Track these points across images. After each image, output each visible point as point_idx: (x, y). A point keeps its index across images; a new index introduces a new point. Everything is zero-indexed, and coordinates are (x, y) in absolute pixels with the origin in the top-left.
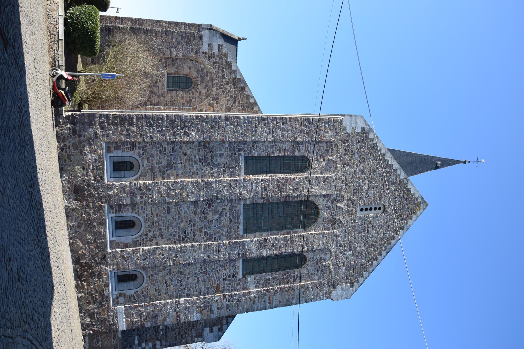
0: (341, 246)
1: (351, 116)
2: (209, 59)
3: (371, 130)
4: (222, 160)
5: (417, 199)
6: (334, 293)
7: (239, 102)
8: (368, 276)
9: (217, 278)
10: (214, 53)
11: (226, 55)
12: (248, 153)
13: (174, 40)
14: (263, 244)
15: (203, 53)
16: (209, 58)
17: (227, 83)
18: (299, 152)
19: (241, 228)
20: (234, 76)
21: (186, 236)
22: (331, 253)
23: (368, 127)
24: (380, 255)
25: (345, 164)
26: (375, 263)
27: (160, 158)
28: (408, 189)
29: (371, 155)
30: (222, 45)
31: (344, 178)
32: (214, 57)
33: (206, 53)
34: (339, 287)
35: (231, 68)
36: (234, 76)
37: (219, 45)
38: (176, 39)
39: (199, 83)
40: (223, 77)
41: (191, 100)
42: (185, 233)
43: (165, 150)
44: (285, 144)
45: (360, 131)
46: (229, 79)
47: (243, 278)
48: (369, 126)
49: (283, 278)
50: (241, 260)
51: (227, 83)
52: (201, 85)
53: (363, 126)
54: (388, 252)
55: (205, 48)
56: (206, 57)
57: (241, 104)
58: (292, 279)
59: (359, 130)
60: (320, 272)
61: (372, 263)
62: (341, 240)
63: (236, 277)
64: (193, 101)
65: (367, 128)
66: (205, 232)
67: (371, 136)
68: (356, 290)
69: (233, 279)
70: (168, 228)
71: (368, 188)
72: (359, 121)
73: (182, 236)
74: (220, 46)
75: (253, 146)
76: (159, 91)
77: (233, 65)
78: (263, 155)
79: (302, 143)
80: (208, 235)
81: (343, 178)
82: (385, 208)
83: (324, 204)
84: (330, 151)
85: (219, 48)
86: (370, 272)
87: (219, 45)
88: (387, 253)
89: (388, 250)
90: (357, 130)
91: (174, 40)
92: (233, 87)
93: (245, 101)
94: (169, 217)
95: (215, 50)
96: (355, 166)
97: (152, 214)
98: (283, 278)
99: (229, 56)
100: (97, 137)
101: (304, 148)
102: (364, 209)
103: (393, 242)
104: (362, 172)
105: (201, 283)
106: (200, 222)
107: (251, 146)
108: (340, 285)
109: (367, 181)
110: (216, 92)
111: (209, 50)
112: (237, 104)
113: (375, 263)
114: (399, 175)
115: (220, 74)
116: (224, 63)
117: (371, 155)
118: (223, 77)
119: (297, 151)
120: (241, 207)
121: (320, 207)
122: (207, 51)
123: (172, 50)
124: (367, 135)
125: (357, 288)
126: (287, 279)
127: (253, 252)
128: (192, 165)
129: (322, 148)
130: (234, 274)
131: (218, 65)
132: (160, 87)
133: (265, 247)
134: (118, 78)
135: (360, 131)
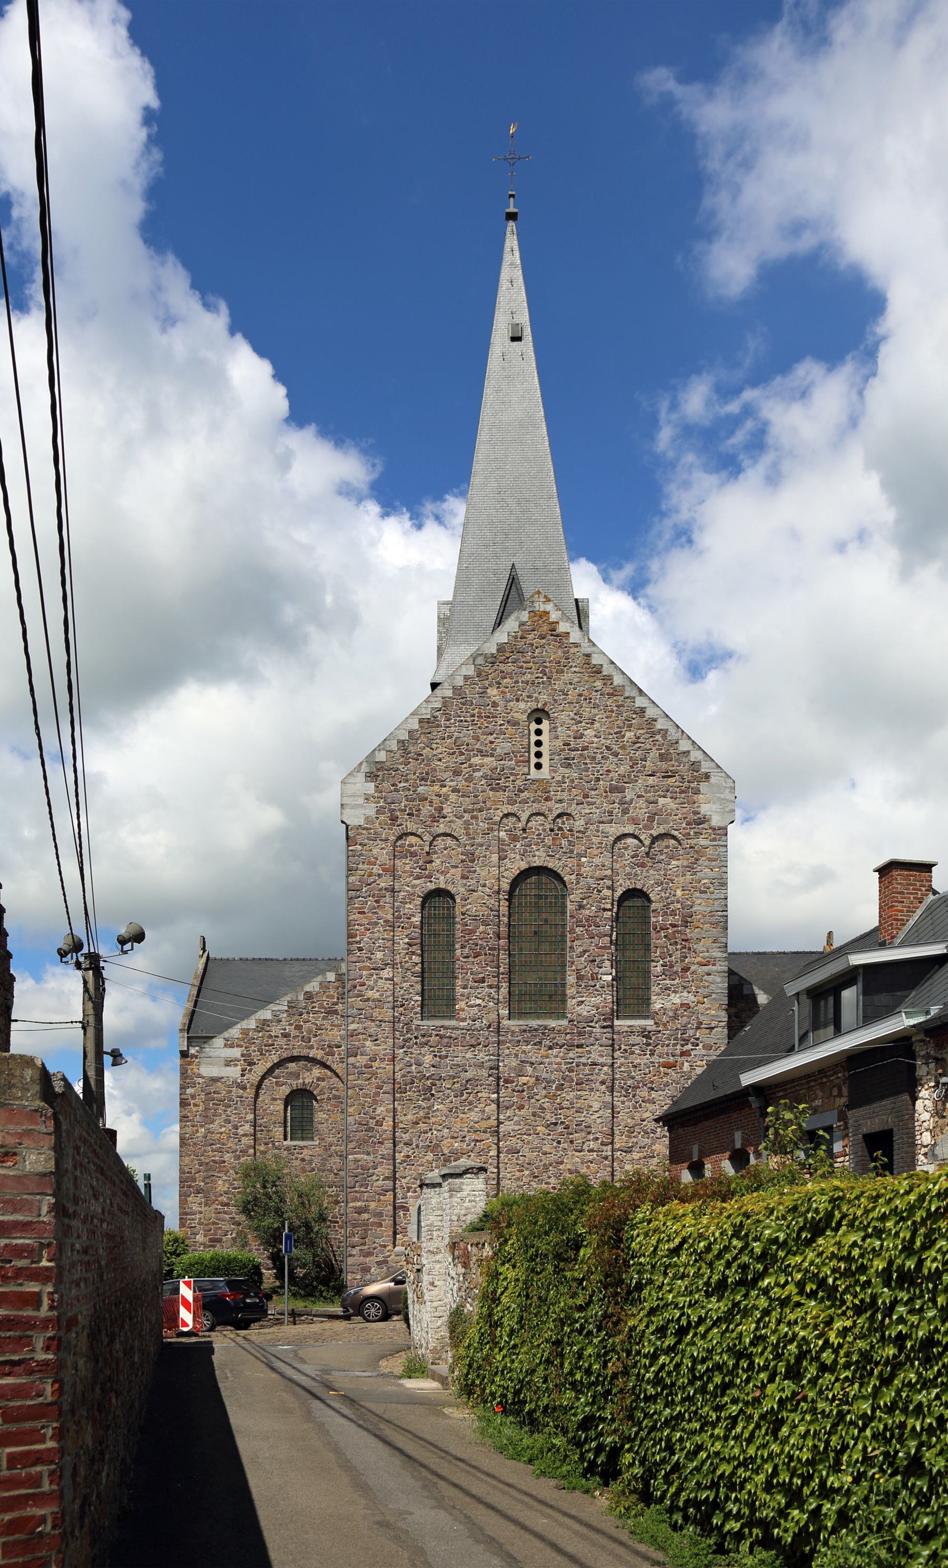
0: (611, 813)
1: (342, 805)
2: (255, 1064)
3: (370, 759)
4: (428, 1059)
5: (522, 624)
6: (716, 821)
7: (336, 1004)
8: (689, 738)
9: (649, 1067)
10: (242, 1055)
11: (245, 1032)
12: (416, 1013)
13: (223, 1130)
14: (587, 981)
15: (243, 1075)
16: (251, 1064)
17: (299, 1028)
18: (413, 916)
19: (552, 1023)
20: (285, 1015)
21: (562, 1123)
22: (625, 836)
23: (365, 764)
24: (643, 710)
25: (440, 814)
26: (659, 725)
27: (423, 1165)
28: (498, 650)
29: (422, 755)
30: (226, 1040)
31: (466, 815)
32: (250, 1055)
33: (243, 1070)
34: (705, 809)
35: (268, 1021)
36: (285, 1015)
37: (226, 1046)
38: (221, 1126)
39: (301, 1081)
40: (286, 1035)
41: (336, 1097)
42: (556, 1124)
43: (408, 1156)
44: (399, 943)
45: (372, 785)
46: (291, 1025)
47: (653, 1019)
48: (361, 764)
49: (665, 937)
50: (616, 1022)
51: (299, 1028)
52: (304, 1078)
53: (361, 777)
54: (640, 691)
55: (234, 1072)
56: (250, 1070)
57: (338, 999)
58: (671, 918)
59: (371, 787)
60: (663, 857)
61: (659, 731)
62: (597, 813)
63: (650, 1032)
64: (336, 1093)
65: (365, 768)
66: (557, 1089)
67: (382, 756)
68: (718, 767)
69: (653, 1038)
70: (545, 1153)
71: (492, 755)
72: (350, 789)
73: (560, 1128)
74: (229, 1044)
75: (402, 1006)
76: (319, 1155)
77: (262, 1018)
78: (418, 987)
79: (396, 910)
80: (563, 1085)
81: (467, 816)
82: (537, 710)
83: (518, 857)
84: (412, 849)
85: (232, 1046)
86: (680, 733)
87: (226, 1046)
88: (641, 691)
89: (634, 693)
90: (369, 792)
91: (223, 1130)
92: (305, 1016)
93: (332, 992)
94: (525, 1150)
95: (236, 1053)
96: (444, 790)
97: (518, 1179)
98: (665, 937)
99: (245, 1026)
100: (385, 1262)
101: (407, 906)
102: (541, 749)
103: (618, 680)
104: (457, 773)
105: (653, 1096)
106: (537, 1097)
107: (401, 1009)
108: (699, 807)
109: (476, 760)
110: (317, 1049)
111: (236, 1065)
112: (339, 1007)
113: (659, 725)
114: (466, 678)
115: (282, 1041)
116: (260, 1034)
117: (422, 755)
118: (286, 1035)
119: (413, 919)
120: (514, 1024)
121: (524, 865)
122: (239, 1068)
123: (242, 1132)
124: (380, 766)
125: (713, 765)
126: (668, 929)
127: (602, 1000)
128: (434, 1111)
129: (407, 868)
130: (643, 1037)
131: (266, 1046)
132: (311, 1153)
133: (594, 977)
134: (290, 1230)
135: (372, 785)
